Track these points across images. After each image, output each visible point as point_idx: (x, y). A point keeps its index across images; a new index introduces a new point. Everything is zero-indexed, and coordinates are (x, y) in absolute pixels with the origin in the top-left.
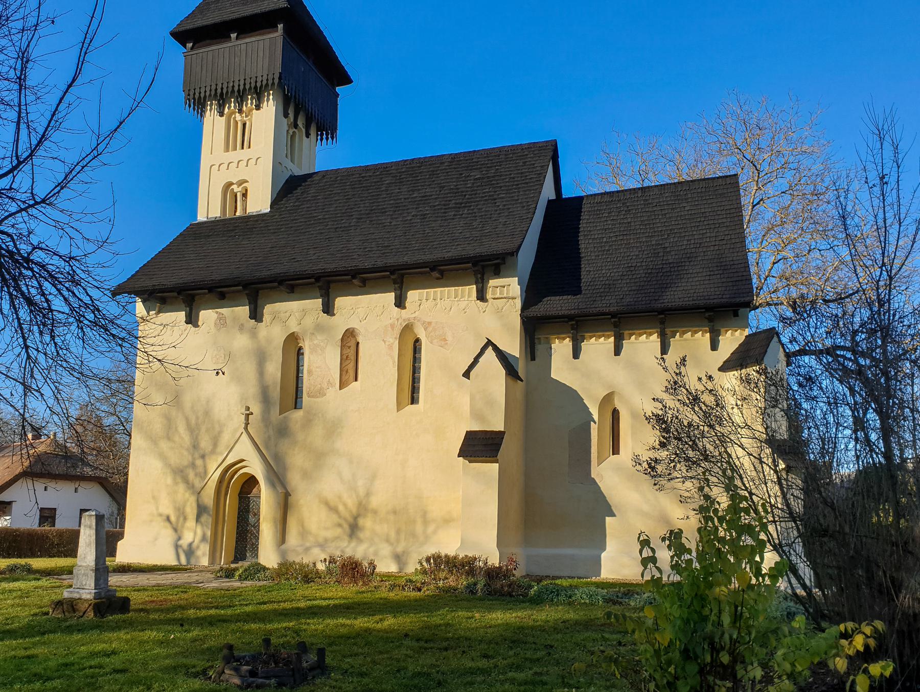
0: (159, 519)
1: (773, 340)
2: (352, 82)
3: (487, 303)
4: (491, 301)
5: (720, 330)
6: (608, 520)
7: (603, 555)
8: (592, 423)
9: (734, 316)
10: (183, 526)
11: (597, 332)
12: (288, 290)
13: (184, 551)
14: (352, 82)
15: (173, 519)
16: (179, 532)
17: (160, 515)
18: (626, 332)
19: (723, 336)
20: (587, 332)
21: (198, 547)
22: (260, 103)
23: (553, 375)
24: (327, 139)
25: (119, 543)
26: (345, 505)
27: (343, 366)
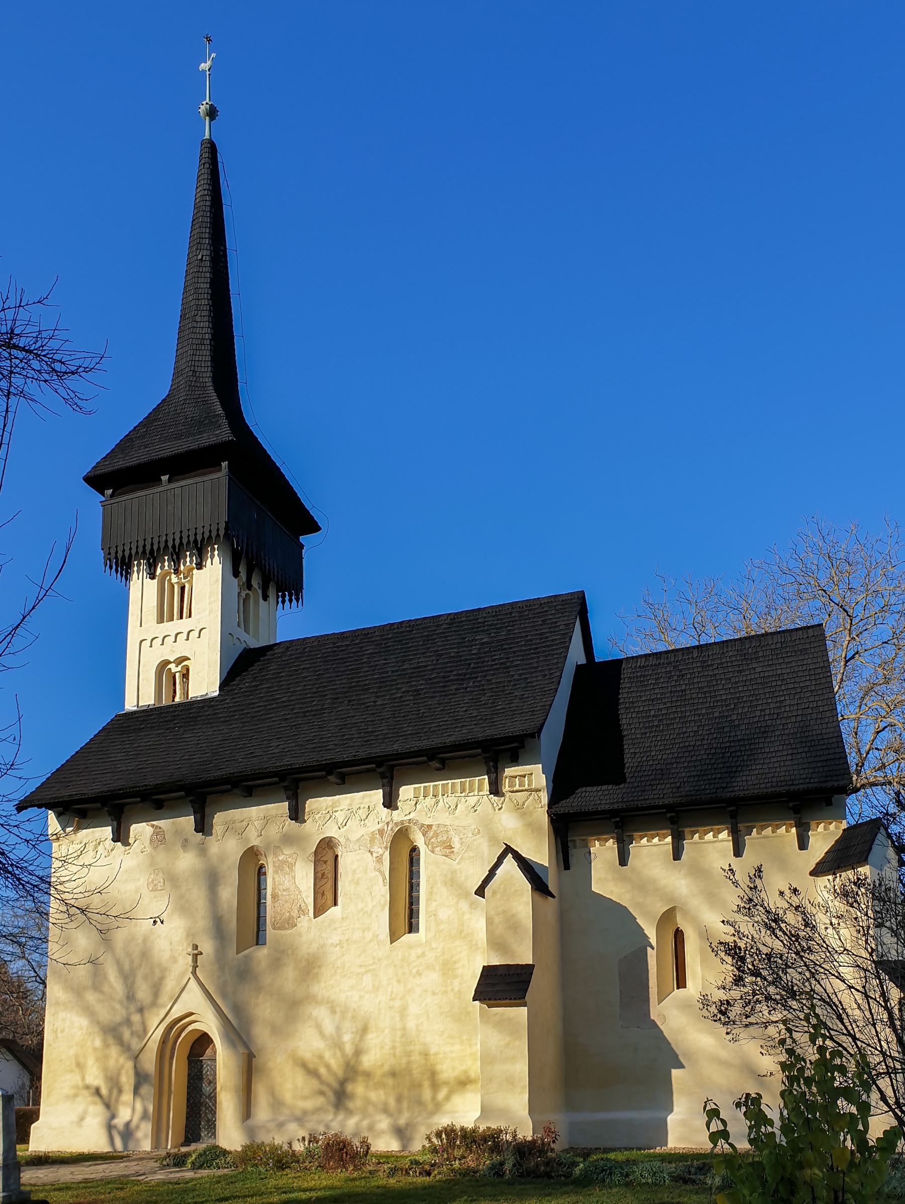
0: (86, 1092)
3: (503, 798)
4: (508, 795)
7: (670, 1118)
8: (649, 949)
10: (117, 1101)
13: (119, 1133)
15: (104, 1091)
16: (112, 1108)
17: (87, 1087)
18: (687, 830)
21: (138, 1127)
26: (328, 1067)
27: (318, 887)
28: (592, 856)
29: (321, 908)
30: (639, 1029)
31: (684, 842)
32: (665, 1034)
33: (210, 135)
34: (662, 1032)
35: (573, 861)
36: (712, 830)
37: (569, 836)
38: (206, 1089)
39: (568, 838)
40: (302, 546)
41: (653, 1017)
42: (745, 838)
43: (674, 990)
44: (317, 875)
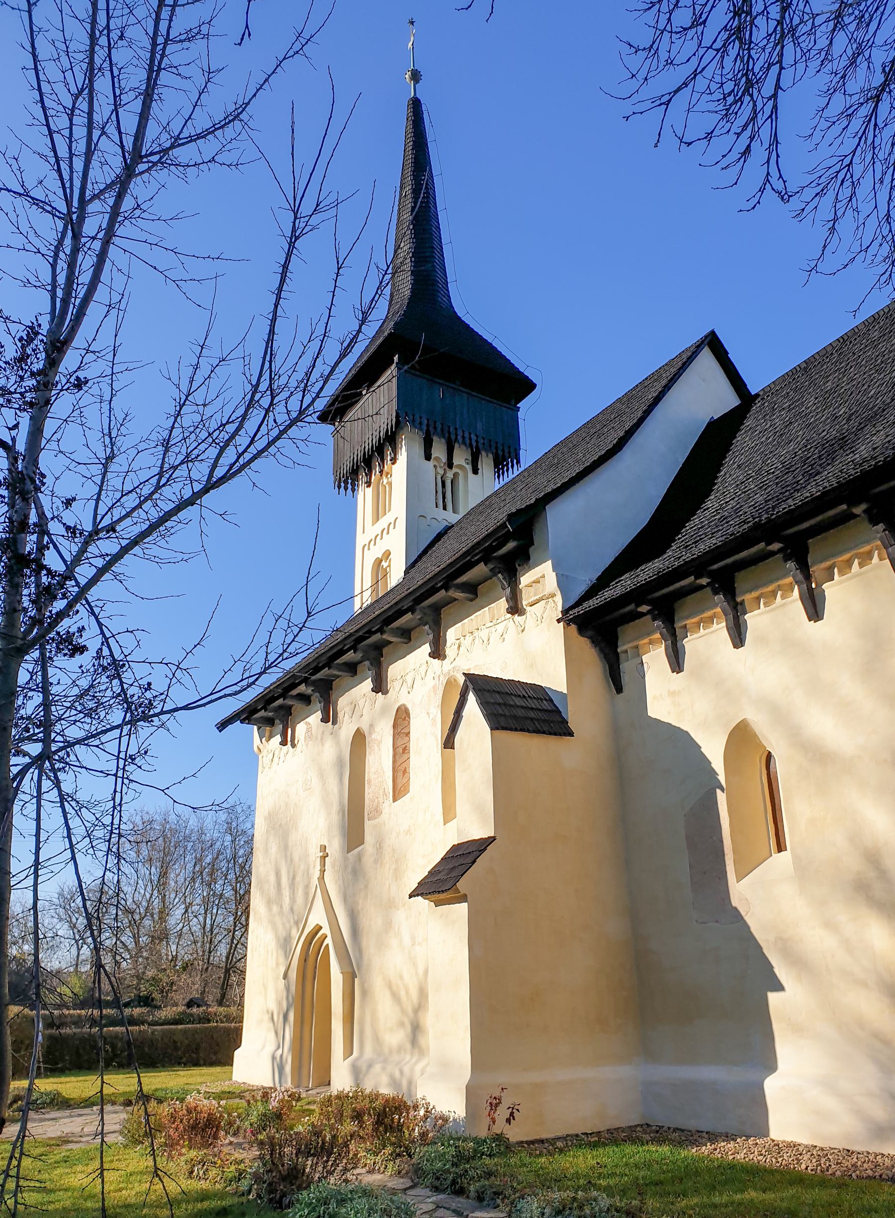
1: (473, 503)
3: (525, 616)
4: (528, 609)
7: (771, 1085)
8: (718, 791)
12: (350, 674)
18: (748, 598)
20: (687, 618)
22: (395, 455)
25: (236, 1052)
27: (398, 764)
28: (645, 665)
29: (402, 789)
31: (746, 617)
32: (753, 930)
33: (415, 94)
38: (806, 1164)
39: (617, 647)
41: (735, 902)
44: (397, 750)
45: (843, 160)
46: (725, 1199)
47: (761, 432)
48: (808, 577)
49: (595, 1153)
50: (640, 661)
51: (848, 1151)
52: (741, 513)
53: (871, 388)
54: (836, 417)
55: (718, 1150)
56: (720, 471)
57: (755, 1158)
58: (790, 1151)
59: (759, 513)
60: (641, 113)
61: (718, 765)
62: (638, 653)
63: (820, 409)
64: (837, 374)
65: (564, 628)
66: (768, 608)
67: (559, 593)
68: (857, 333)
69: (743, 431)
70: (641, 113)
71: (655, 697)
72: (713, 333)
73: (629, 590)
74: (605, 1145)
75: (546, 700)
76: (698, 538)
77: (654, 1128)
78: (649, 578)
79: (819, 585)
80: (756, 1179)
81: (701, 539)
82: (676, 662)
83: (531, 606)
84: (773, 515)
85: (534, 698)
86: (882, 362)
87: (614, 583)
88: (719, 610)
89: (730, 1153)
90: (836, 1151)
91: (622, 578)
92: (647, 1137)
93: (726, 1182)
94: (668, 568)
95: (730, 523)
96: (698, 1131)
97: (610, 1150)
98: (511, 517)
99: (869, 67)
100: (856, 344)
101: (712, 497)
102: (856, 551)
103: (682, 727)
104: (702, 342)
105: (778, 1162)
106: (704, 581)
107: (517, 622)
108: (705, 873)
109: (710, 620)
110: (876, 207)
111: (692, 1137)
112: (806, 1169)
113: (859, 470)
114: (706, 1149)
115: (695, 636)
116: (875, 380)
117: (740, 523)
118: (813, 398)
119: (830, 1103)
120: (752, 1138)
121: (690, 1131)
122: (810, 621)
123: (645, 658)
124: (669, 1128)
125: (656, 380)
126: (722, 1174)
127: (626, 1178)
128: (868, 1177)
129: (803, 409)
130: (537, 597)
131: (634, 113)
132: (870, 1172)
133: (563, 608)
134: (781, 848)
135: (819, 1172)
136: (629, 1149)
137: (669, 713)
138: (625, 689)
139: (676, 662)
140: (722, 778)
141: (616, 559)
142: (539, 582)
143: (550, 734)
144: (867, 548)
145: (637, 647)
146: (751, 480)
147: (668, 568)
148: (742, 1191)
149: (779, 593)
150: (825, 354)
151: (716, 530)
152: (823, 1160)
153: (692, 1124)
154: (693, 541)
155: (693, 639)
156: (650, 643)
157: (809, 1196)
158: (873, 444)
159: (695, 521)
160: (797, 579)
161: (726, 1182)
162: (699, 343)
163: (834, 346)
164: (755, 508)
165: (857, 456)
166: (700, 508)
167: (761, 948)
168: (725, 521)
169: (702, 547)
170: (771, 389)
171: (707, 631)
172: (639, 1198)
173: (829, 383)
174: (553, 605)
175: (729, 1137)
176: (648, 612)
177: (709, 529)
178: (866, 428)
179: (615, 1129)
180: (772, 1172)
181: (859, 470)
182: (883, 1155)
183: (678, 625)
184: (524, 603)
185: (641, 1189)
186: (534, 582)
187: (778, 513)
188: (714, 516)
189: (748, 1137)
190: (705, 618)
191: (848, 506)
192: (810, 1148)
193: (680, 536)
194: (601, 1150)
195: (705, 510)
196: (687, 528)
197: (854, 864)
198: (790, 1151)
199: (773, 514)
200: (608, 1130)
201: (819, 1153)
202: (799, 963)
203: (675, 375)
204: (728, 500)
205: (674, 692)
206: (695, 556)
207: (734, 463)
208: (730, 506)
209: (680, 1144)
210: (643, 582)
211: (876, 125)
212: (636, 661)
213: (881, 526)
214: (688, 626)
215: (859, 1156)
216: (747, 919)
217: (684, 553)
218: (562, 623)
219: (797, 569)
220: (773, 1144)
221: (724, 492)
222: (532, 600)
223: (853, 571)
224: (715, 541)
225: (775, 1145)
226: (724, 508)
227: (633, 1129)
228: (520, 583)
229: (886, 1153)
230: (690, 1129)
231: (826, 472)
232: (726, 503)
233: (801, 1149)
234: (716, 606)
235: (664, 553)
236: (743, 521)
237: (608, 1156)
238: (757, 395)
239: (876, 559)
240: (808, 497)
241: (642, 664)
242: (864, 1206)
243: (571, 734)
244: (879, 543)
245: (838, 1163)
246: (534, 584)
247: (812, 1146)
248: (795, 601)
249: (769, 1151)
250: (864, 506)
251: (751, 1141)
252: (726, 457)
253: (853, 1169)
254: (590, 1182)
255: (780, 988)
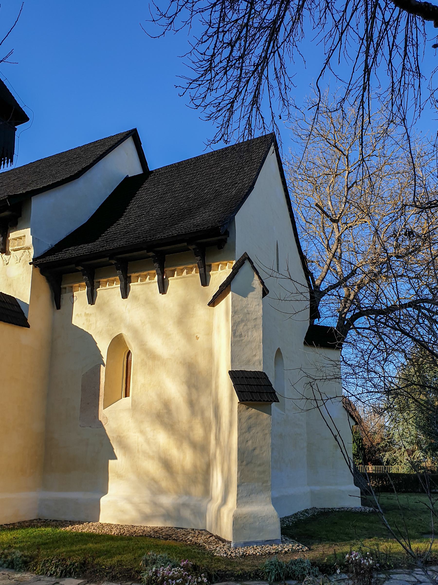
2: (28, 119)
3: (9, 256)
4: (12, 252)
5: (211, 265)
6: (111, 462)
7: (104, 500)
8: (102, 366)
9: (219, 249)
11: (110, 277)
14: (28, 119)
18: (133, 275)
19: (214, 270)
20: (101, 278)
23: (73, 323)
24: (8, 163)
28: (75, 298)
30: (90, 428)
31: (131, 284)
34: (105, 430)
35: (63, 303)
36: (149, 274)
37: (62, 284)
38: (114, 532)
39: (61, 285)
40: (16, 129)
41: (100, 418)
42: (169, 279)
43: (122, 398)
45: (230, 99)
46: (78, 548)
47: (152, 192)
48: (163, 273)
49: (12, 533)
50: (72, 295)
51: (133, 526)
52: (137, 232)
53: (206, 189)
54: (188, 198)
55: (74, 528)
56: (128, 206)
57: (92, 531)
58: (107, 528)
59: (146, 235)
60: (183, 88)
61: (104, 353)
62: (72, 290)
63: (181, 191)
64: (192, 175)
65: (33, 268)
66: (142, 283)
67: (33, 248)
68: (204, 158)
69: (142, 189)
70: (183, 88)
71: (77, 315)
72: (135, 130)
73: (73, 256)
74: (17, 529)
75: (16, 306)
76: (114, 239)
77: (43, 520)
78: (85, 253)
79: (167, 277)
80: (92, 539)
81: (115, 240)
82: (92, 299)
83: (14, 251)
84: (152, 239)
85: (10, 303)
86: (213, 178)
87: (64, 250)
88: (118, 278)
89: (80, 529)
90: (127, 526)
91: (69, 249)
92: (39, 525)
93: (79, 541)
94: (97, 250)
95: (131, 236)
96: (65, 521)
97: (19, 531)
98: (10, 197)
99: (250, 62)
100: (203, 164)
101: (123, 219)
102: (186, 266)
103: (89, 332)
104: (130, 133)
105: (102, 532)
106: (113, 262)
107: (4, 258)
108: (88, 404)
109: (113, 282)
110: (239, 127)
111: (64, 523)
112: (114, 534)
113: (195, 229)
114: (68, 529)
115: (104, 288)
116: (208, 186)
117: (136, 237)
118: (179, 184)
119: (128, 507)
120: (91, 523)
121: (61, 521)
122: (160, 293)
123: (75, 294)
124: (51, 520)
125: (102, 145)
126: (77, 538)
127: (29, 543)
128: (140, 536)
129: (173, 188)
130: (19, 247)
131: (180, 86)
132: (141, 534)
133: (33, 257)
134: (127, 395)
135: (119, 535)
136: (30, 530)
137: (84, 324)
138: (62, 308)
139: (92, 299)
140: (105, 360)
141: (67, 237)
142: (21, 239)
143: (17, 325)
144: (191, 266)
145: (72, 287)
146: (143, 216)
147: (97, 250)
148: (86, 544)
149: (148, 277)
150: (188, 162)
151: (123, 237)
152: (122, 530)
153: (62, 518)
154: (111, 239)
155: (102, 289)
156: (79, 286)
157: (116, 544)
158: (203, 218)
159: (112, 229)
160: (158, 272)
161: (79, 541)
162: (128, 133)
163: (193, 160)
164: (144, 232)
165: (195, 221)
166: (115, 223)
167: (109, 440)
168: (128, 234)
169: (116, 245)
170: (159, 171)
171: (110, 287)
172: (37, 550)
173: (187, 179)
174: (28, 254)
175: (80, 523)
176: (82, 270)
177: (120, 236)
178: (201, 208)
179: (22, 522)
180: (98, 536)
181: (195, 229)
182: (147, 527)
183: (95, 281)
184: (10, 248)
185: (38, 546)
186: (18, 238)
187: (155, 238)
188: (123, 229)
189: (89, 522)
190: (110, 280)
191: (187, 244)
192: (116, 526)
193: (104, 235)
194: (15, 531)
195: (118, 224)
196: (108, 231)
197: (158, 406)
198: (107, 528)
199: (153, 238)
200: (19, 522)
201: (120, 527)
202: (125, 447)
203: (113, 146)
204: (131, 223)
205: (88, 314)
206: (111, 248)
207: (136, 204)
208: (132, 227)
209: (56, 527)
210: (82, 254)
211: (246, 90)
212: (70, 294)
213: (199, 258)
214: (101, 282)
215: (137, 528)
216: (105, 427)
217: (105, 245)
218: (32, 265)
219: (159, 267)
220: (100, 525)
221: (129, 218)
222: (16, 248)
223: (183, 275)
224: (122, 243)
225: (101, 525)
226: (129, 226)
227: (32, 521)
228: (9, 237)
229: (148, 526)
230: (61, 520)
231: (180, 225)
232: (130, 224)
233: (112, 526)
234: (117, 276)
235: (95, 241)
236: (138, 237)
237: (20, 534)
238: (152, 172)
239: (194, 272)
240: (170, 235)
241: (73, 296)
242: (138, 547)
243: (28, 326)
244: (197, 265)
245: (128, 531)
246: (18, 239)
247: (118, 525)
248: (155, 282)
249: (98, 527)
250: (194, 247)
251: (90, 524)
252: (132, 200)
253: (134, 533)
254: (10, 546)
255: (115, 458)
